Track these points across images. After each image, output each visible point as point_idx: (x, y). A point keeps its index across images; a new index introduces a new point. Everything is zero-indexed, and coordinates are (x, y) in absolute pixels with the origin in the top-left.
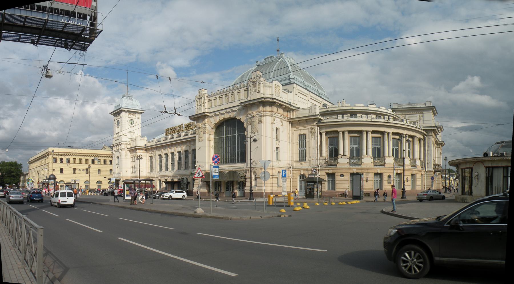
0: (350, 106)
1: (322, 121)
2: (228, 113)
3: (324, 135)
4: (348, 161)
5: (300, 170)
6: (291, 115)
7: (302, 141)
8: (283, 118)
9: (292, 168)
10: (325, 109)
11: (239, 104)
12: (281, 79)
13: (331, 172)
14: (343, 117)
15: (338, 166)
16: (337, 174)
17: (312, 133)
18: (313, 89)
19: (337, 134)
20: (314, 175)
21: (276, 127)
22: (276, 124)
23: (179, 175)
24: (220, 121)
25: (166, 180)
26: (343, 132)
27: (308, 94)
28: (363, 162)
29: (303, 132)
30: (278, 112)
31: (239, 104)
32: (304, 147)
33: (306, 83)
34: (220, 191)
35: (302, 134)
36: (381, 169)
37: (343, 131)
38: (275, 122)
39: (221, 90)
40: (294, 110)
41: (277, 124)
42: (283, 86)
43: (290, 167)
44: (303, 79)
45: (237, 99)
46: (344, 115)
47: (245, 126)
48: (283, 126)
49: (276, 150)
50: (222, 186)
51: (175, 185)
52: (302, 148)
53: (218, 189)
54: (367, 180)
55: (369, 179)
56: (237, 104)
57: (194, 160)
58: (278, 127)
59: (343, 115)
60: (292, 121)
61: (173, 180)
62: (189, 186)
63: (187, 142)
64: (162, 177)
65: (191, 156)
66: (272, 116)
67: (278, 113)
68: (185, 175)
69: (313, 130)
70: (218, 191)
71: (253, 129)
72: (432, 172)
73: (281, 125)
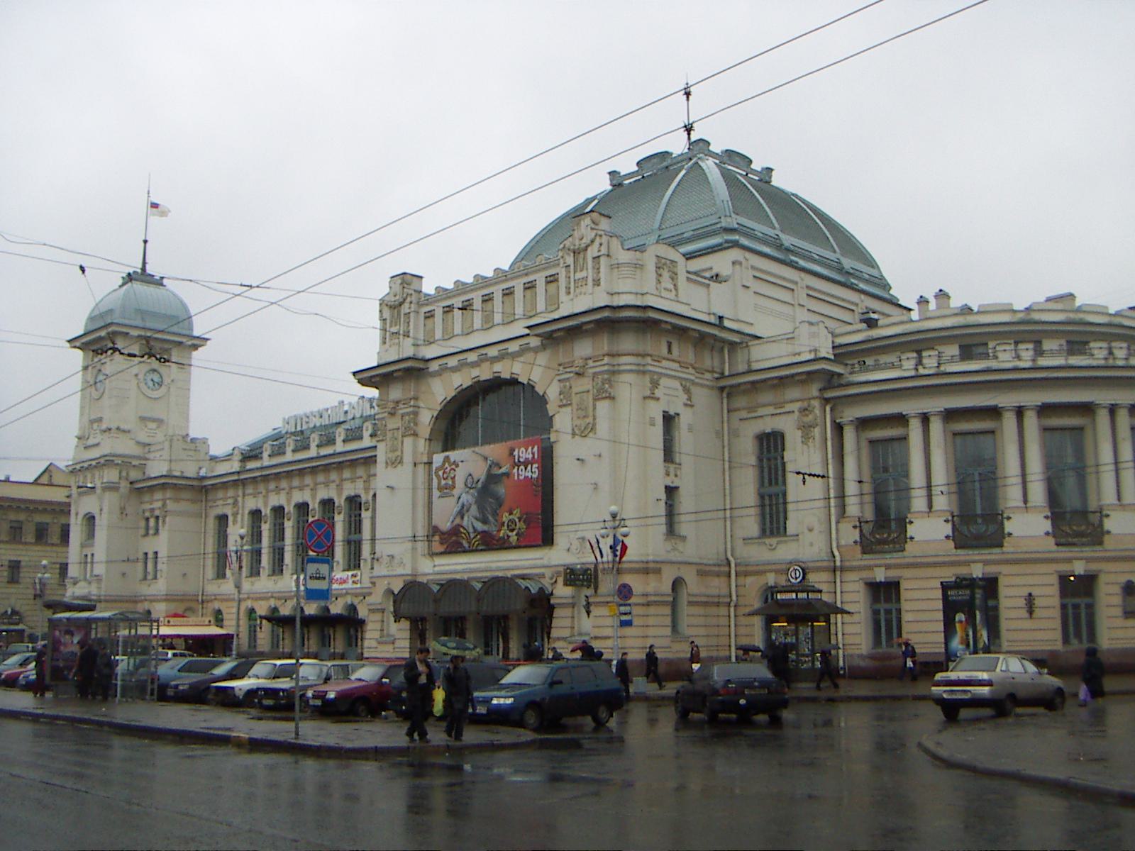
0: (1062, 311)
1: (843, 381)
2: (453, 372)
3: (849, 435)
4: (948, 529)
5: (764, 572)
6: (727, 365)
7: (769, 459)
8: (692, 378)
9: (733, 565)
10: (859, 331)
11: (527, 331)
12: (692, 233)
13: (880, 575)
14: (919, 362)
15: (1008, 545)
16: (1103, 579)
17: (806, 429)
18: (822, 262)
19: (904, 427)
20: (792, 592)
21: (664, 412)
22: (664, 399)
23: (252, 596)
24: (463, 390)
25: (275, 610)
26: (925, 419)
27: (796, 283)
28: (913, 535)
29: (768, 425)
30: (670, 356)
31: (527, 331)
32: (777, 483)
33: (787, 240)
34: (506, 657)
35: (769, 434)
36: (1088, 560)
37: (925, 414)
38: (658, 393)
39: (756, 233)
40: (736, 343)
41: (1018, 357)
42: (687, 259)
43: (727, 559)
44: (776, 225)
45: (519, 311)
46: (925, 354)
47: (551, 408)
48: (692, 406)
49: (663, 497)
50: (511, 636)
51: (308, 632)
52: (770, 484)
53: (498, 645)
54: (1031, 607)
55: (1038, 602)
56: (518, 329)
57: (223, 550)
58: (672, 413)
59: (919, 352)
60: (731, 386)
61: (328, 610)
62: (359, 634)
63: (166, 488)
64: (261, 599)
65: (293, 527)
66: (644, 373)
67: (668, 360)
68: (347, 594)
69: (807, 415)
70: (498, 654)
71: (578, 422)
72: (233, 600)
73: (686, 405)
